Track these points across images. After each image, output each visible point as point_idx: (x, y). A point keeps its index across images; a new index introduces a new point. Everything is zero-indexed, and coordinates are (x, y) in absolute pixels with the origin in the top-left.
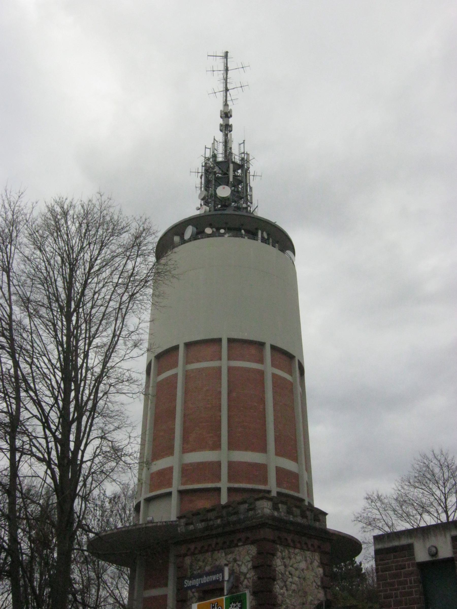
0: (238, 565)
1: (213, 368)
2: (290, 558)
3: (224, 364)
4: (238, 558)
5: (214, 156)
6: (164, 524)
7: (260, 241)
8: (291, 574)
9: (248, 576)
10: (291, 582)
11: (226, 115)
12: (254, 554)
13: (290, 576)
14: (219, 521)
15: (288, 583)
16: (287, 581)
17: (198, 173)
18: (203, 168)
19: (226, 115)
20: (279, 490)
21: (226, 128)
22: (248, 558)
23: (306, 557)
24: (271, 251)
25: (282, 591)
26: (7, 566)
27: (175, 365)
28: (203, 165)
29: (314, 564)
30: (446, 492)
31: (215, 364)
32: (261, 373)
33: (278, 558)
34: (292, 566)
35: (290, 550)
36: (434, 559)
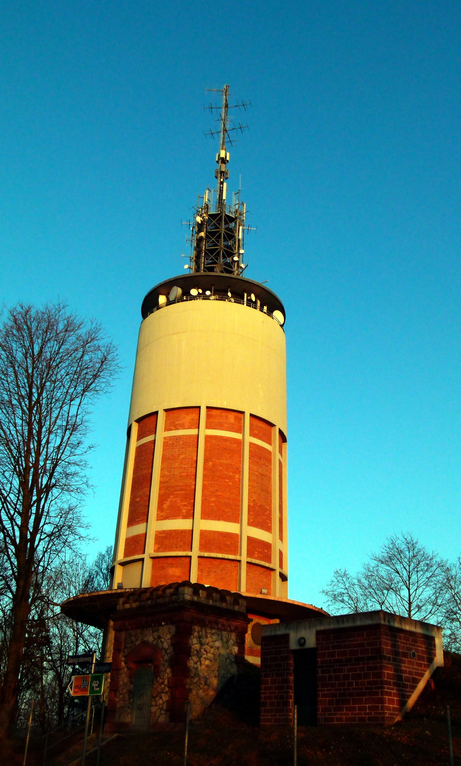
0: (161, 641)
1: (190, 436)
2: (207, 637)
4: (162, 636)
6: (132, 590)
7: (245, 305)
8: (206, 652)
9: (168, 651)
10: (205, 658)
12: (174, 633)
13: (205, 653)
14: (149, 602)
15: (202, 659)
16: (201, 657)
20: (250, 560)
22: (169, 636)
23: (222, 637)
25: (195, 665)
26: (183, 513)
29: (230, 642)
30: (411, 570)
31: (193, 432)
33: (194, 637)
34: (207, 644)
35: (207, 631)
36: (302, 647)
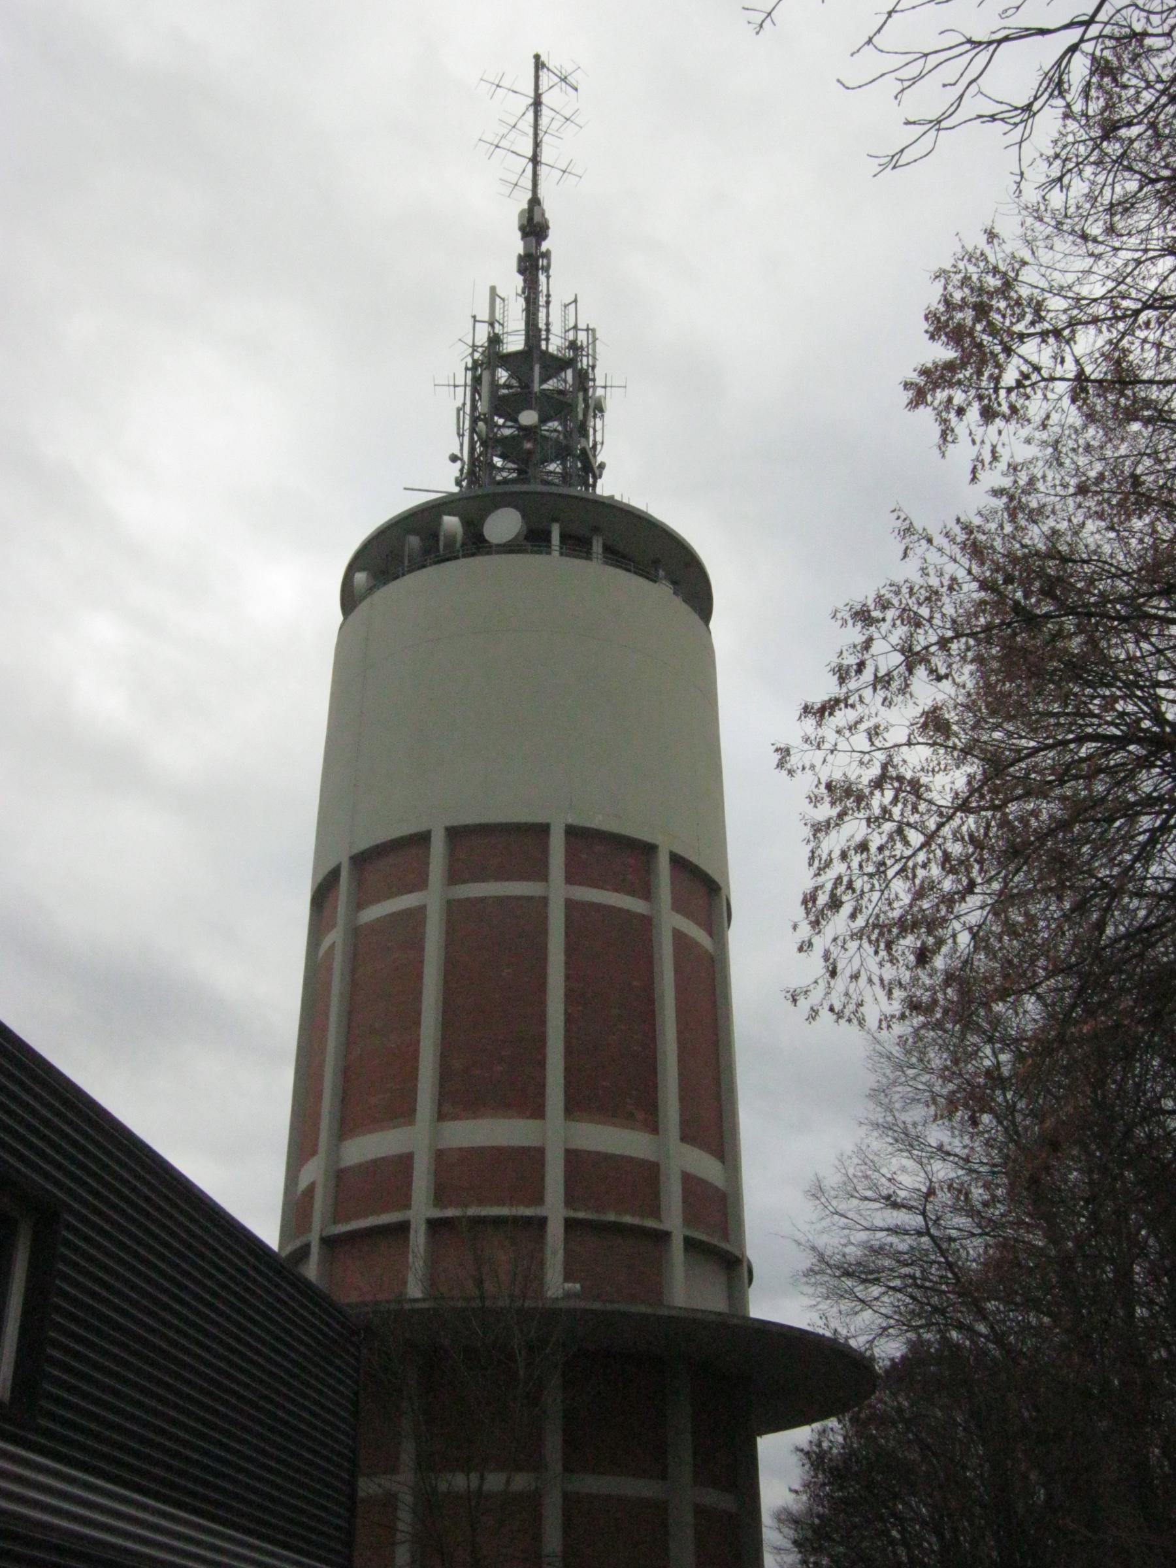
3: (558, 890)
5: (495, 340)
7: (556, 554)
11: (534, 227)
17: (455, 386)
18: (469, 374)
19: (534, 227)
21: (532, 265)
24: (658, 596)
27: (421, 883)
28: (470, 365)
32: (646, 923)
